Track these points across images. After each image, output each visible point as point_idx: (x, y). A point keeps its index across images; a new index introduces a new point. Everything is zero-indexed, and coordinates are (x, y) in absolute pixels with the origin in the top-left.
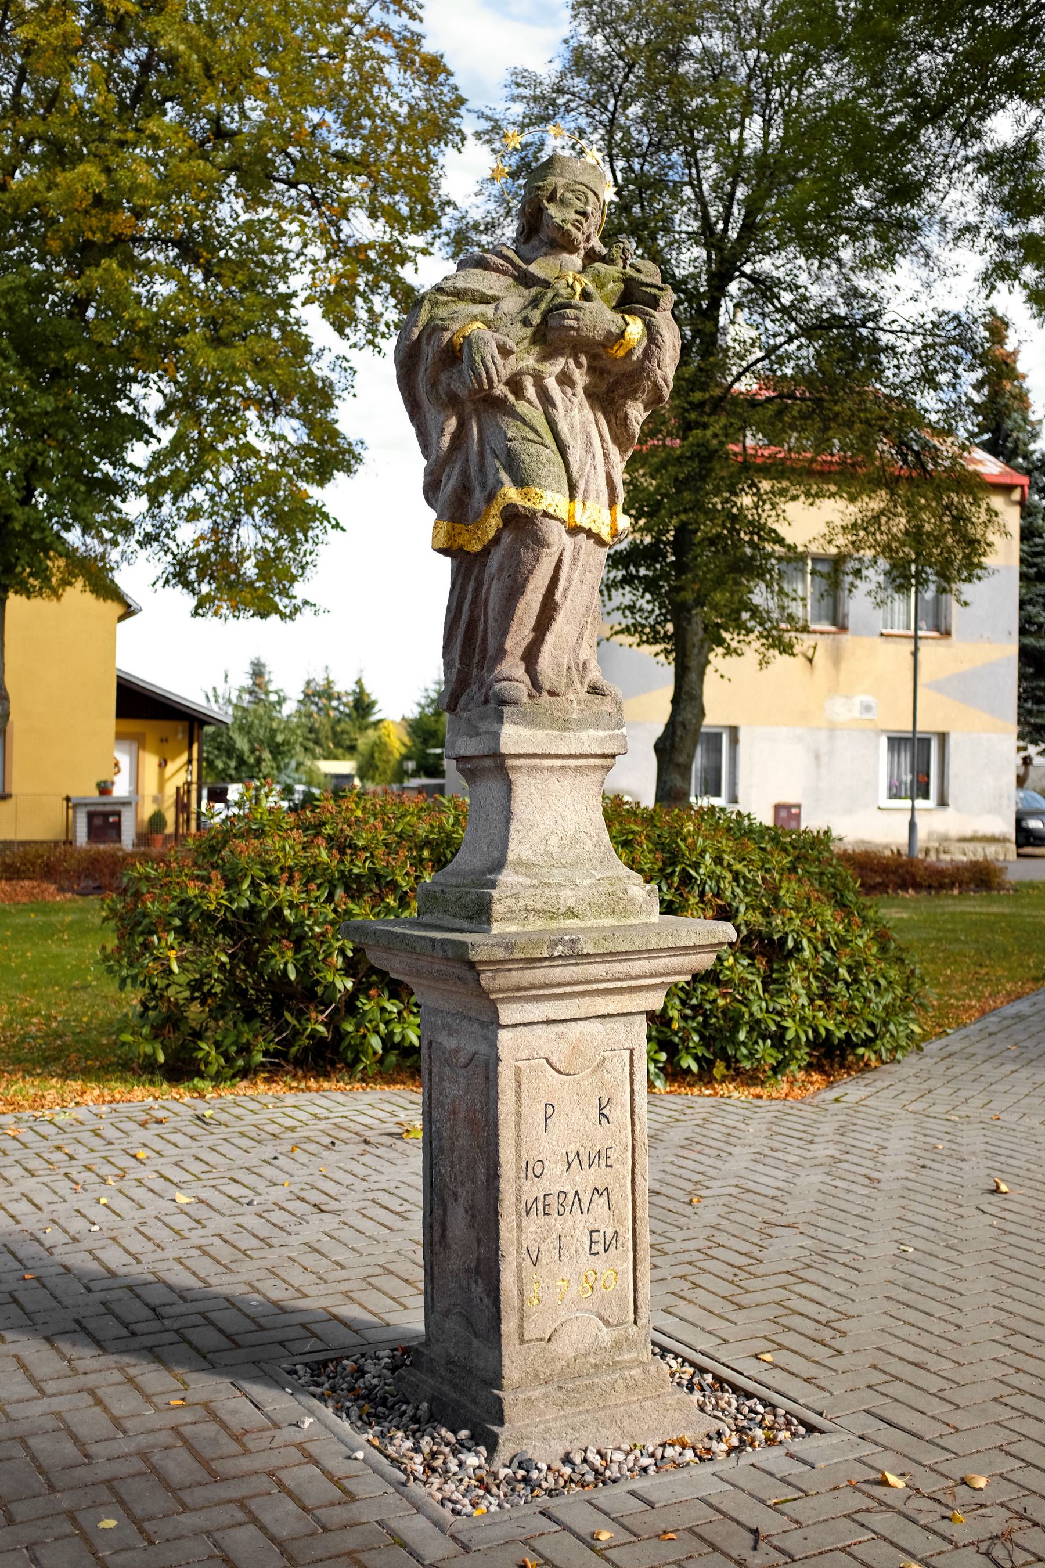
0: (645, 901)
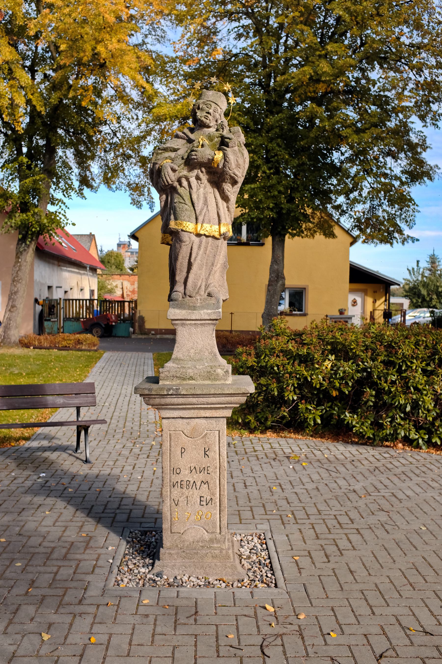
0: (223, 375)
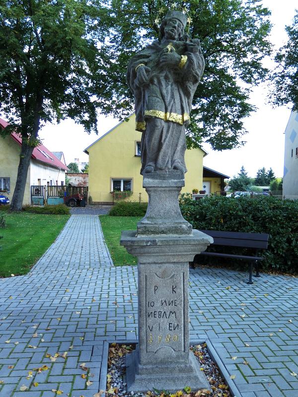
0: (187, 230)
